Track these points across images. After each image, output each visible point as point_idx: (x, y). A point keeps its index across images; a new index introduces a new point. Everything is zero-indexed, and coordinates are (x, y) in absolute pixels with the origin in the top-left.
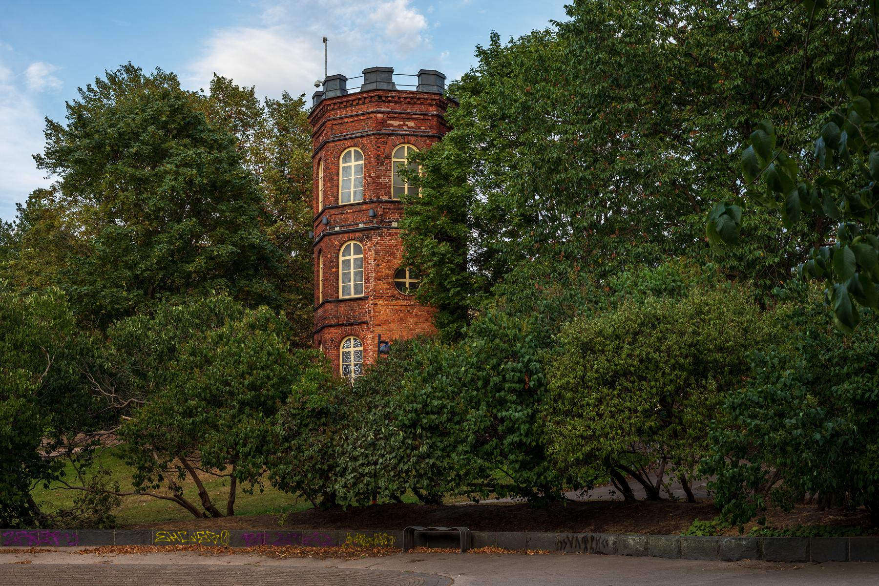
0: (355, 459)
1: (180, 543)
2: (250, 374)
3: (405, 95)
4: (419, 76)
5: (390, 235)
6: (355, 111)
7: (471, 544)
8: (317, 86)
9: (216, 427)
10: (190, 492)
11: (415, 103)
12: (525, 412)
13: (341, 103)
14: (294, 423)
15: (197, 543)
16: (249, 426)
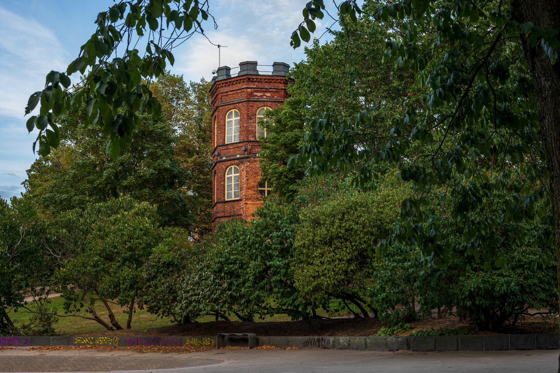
0: (188, 292)
1: (89, 344)
2: (130, 242)
3: (264, 78)
4: (273, 66)
5: (255, 161)
6: (235, 87)
7: (257, 344)
8: (214, 73)
9: (108, 273)
10: (104, 315)
11: (271, 82)
12: (284, 262)
13: (227, 83)
14: (153, 271)
15: (99, 344)
16: (127, 272)
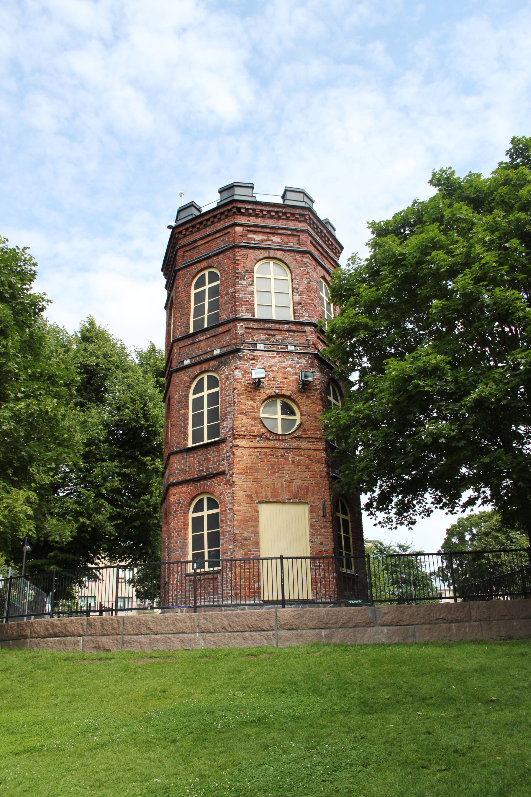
3: (267, 209)
5: (254, 358)
